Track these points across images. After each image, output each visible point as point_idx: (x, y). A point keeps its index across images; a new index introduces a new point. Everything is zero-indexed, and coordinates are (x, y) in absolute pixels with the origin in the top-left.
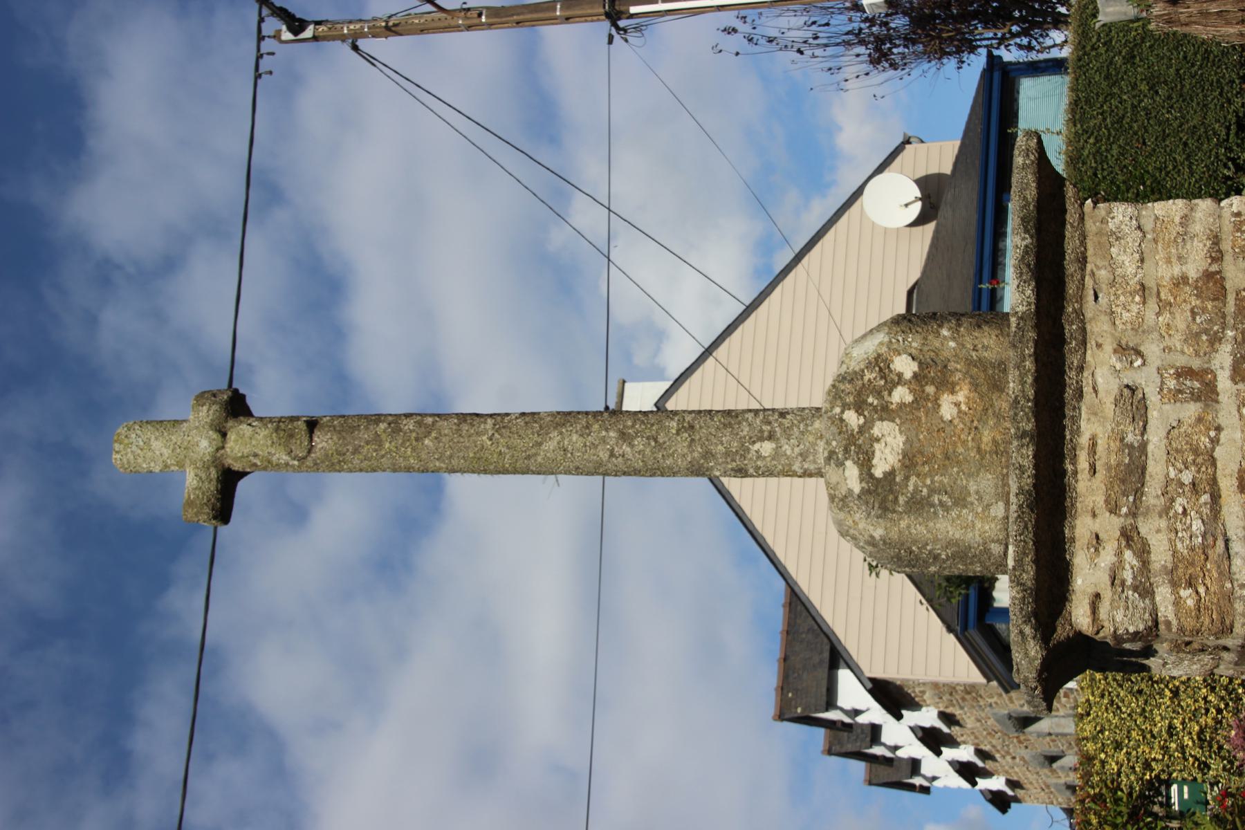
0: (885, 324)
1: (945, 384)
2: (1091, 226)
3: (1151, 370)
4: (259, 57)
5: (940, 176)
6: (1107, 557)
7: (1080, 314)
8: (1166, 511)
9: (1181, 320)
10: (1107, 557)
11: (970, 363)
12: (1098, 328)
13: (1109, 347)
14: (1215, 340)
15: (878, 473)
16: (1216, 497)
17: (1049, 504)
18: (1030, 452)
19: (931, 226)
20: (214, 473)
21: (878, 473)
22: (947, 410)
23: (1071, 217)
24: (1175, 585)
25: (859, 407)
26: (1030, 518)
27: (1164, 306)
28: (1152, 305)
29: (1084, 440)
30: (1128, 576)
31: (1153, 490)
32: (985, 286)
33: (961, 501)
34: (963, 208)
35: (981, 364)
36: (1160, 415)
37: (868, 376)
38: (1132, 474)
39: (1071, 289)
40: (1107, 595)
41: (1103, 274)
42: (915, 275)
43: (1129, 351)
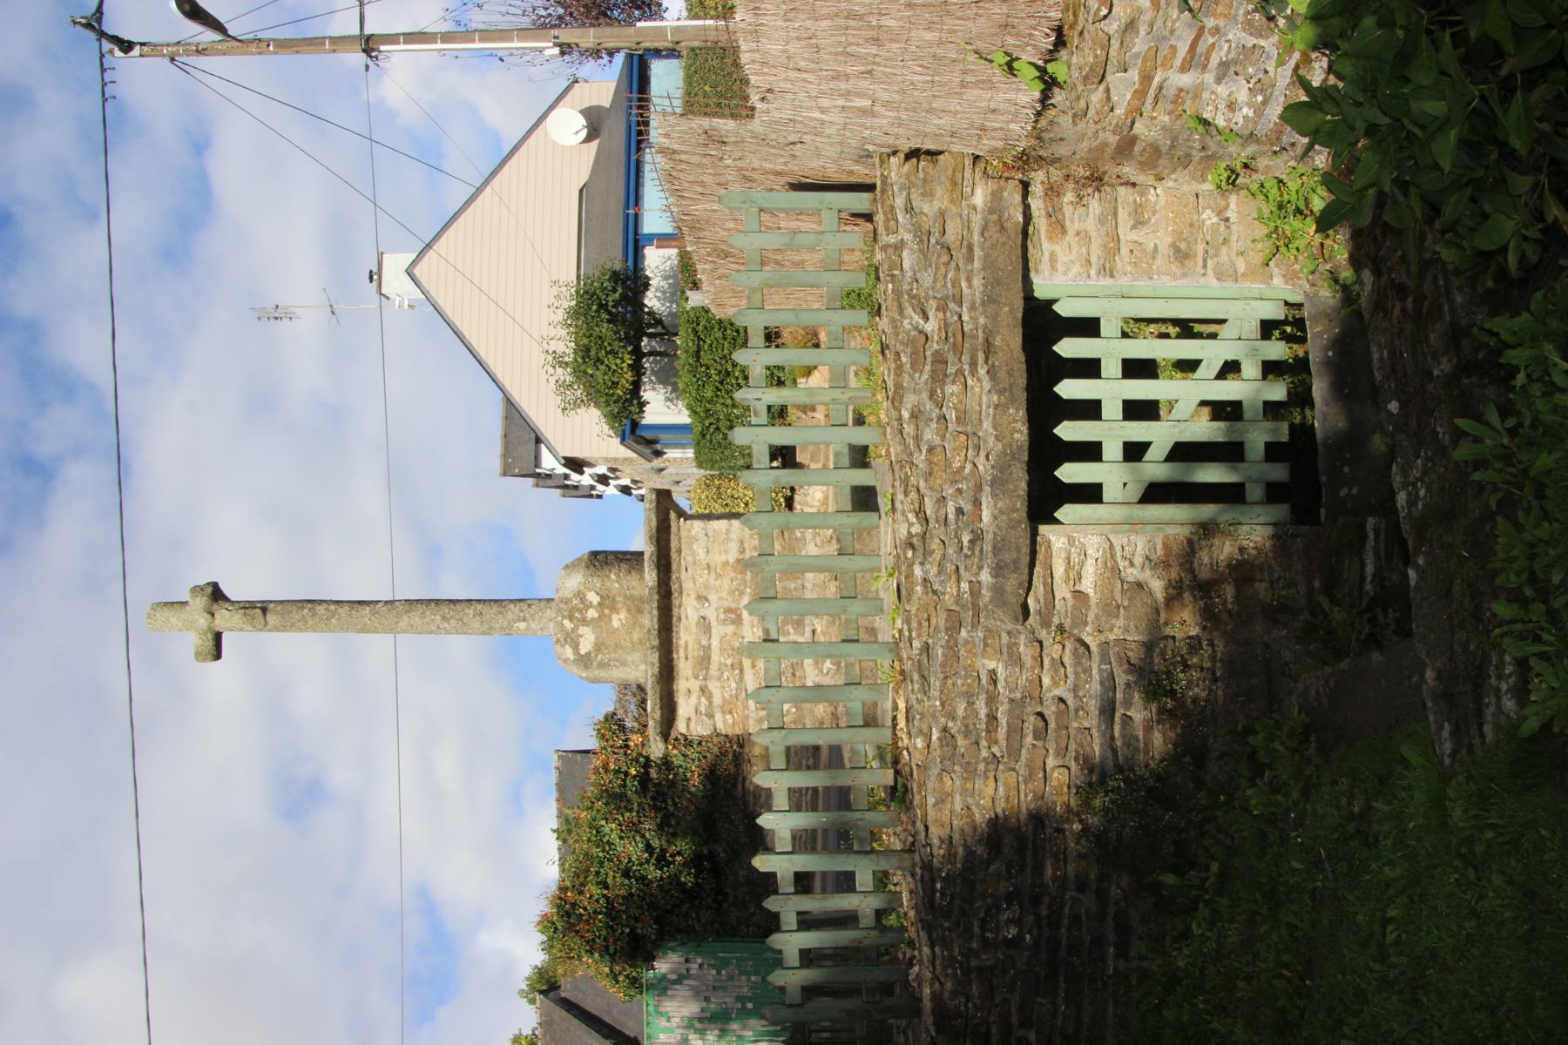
0: (580, 559)
1: (614, 609)
2: (683, 533)
3: (712, 609)
4: (104, 85)
5: (599, 109)
6: (693, 700)
7: (678, 578)
8: (720, 678)
9: (726, 582)
10: (693, 700)
11: (626, 597)
12: (688, 586)
13: (693, 596)
14: (742, 593)
15: (583, 652)
16: (742, 671)
17: (667, 673)
18: (656, 655)
19: (595, 144)
20: (210, 636)
21: (583, 652)
22: (616, 623)
23: (674, 529)
24: (723, 713)
25: (571, 618)
26: (658, 688)
27: (719, 576)
28: (713, 575)
29: (682, 642)
30: (703, 709)
31: (714, 667)
32: (631, 211)
33: (624, 664)
34: (616, 131)
35: (632, 598)
36: (718, 631)
37: (575, 602)
38: (704, 660)
39: (674, 567)
40: (694, 718)
41: (689, 558)
42: (584, 178)
43: (702, 598)
